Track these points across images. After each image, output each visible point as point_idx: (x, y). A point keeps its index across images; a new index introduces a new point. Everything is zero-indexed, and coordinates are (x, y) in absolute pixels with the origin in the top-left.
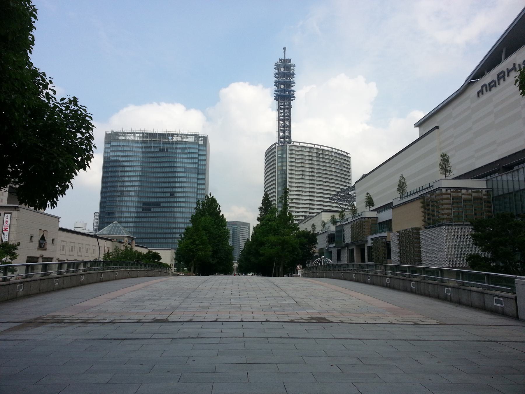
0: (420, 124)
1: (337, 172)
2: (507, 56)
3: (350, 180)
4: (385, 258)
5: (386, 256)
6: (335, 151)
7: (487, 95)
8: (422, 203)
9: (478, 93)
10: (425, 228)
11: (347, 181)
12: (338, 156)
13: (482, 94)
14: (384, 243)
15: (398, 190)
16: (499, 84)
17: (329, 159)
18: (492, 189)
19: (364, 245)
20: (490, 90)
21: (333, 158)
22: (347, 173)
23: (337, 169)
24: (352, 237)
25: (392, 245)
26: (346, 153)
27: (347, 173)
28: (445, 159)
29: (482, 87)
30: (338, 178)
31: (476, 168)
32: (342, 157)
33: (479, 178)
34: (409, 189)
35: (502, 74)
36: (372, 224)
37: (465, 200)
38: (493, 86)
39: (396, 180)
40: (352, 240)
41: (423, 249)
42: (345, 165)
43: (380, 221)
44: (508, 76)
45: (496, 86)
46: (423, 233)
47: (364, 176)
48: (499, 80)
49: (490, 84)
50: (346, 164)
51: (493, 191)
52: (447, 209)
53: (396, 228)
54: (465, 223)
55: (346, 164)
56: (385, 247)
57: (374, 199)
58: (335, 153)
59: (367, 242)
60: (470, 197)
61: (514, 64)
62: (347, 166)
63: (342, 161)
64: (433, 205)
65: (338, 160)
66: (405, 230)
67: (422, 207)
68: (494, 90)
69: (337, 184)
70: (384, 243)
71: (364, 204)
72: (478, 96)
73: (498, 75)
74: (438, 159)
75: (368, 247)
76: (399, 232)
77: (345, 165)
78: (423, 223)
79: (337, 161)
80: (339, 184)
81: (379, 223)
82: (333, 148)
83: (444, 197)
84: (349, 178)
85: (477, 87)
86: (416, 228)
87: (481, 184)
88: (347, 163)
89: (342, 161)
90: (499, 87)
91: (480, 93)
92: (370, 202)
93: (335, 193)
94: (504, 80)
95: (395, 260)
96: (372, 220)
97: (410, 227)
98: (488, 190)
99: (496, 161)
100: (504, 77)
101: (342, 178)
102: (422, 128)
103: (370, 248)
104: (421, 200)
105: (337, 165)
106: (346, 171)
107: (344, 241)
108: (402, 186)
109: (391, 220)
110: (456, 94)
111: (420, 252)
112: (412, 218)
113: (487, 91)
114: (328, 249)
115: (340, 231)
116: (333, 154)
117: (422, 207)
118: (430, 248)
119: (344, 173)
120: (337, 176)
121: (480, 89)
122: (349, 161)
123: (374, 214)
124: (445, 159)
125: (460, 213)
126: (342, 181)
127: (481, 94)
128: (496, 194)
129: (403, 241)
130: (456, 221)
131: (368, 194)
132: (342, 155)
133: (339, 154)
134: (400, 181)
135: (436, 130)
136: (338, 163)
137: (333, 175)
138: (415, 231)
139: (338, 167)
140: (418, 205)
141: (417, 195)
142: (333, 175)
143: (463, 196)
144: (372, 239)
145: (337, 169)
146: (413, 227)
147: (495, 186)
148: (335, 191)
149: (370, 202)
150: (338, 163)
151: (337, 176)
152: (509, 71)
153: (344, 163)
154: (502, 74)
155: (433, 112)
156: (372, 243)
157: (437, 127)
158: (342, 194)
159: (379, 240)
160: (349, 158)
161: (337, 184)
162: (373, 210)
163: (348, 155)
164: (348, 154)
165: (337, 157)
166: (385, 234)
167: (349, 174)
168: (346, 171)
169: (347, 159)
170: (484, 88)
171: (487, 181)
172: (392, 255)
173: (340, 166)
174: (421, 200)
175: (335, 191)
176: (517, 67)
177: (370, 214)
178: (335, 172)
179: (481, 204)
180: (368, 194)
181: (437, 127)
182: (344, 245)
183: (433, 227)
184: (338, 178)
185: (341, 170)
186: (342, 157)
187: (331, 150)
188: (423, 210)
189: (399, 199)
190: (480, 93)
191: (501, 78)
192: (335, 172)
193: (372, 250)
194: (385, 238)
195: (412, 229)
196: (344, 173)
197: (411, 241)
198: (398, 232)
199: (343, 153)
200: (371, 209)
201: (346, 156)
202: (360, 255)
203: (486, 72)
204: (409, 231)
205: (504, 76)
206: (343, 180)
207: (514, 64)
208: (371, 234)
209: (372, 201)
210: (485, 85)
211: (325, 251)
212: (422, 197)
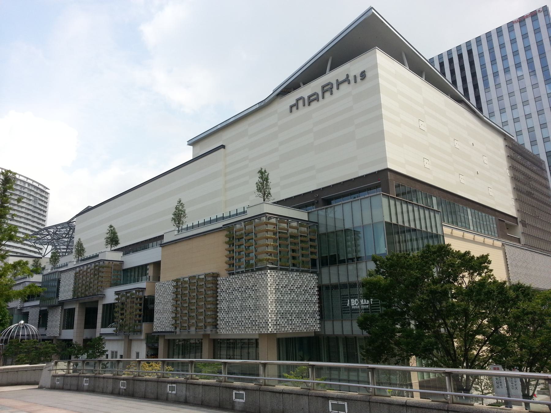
0: (194, 143)
1: (29, 209)
2: (332, 69)
3: (45, 221)
4: (139, 321)
5: (141, 318)
6: (31, 182)
7: (303, 111)
8: (226, 236)
9: (291, 107)
10: (230, 274)
11: (41, 217)
12: (33, 189)
13: (297, 109)
14: (141, 299)
15: (173, 219)
16: (323, 98)
17: (21, 191)
18: (317, 224)
19: (97, 302)
20: (309, 105)
21: (26, 190)
22: (42, 213)
23: (29, 205)
24: (74, 291)
25: (156, 301)
26: (45, 187)
27: (42, 213)
28: (264, 176)
29: (298, 100)
30: (29, 217)
31: (281, 199)
32: (39, 192)
33: (300, 207)
34: (188, 222)
35: (329, 86)
36: (114, 270)
37: (292, 236)
38: (313, 100)
39: (171, 205)
40: (74, 295)
41: (222, 305)
42: (41, 202)
43: (127, 266)
44: (338, 89)
45: (318, 101)
46: (223, 283)
47: (88, 209)
48: (323, 93)
49: (309, 97)
50: (42, 201)
51: (318, 227)
52: (267, 246)
53: (168, 275)
54: (301, 269)
55: (42, 201)
56: (141, 304)
57: (119, 235)
58: (29, 184)
59: (103, 297)
60: (295, 231)
61: (348, 76)
62: (43, 203)
63: (38, 196)
64: (243, 242)
65: (32, 193)
66: (190, 278)
67: (226, 243)
68: (314, 104)
69: (27, 224)
70: (141, 299)
71: (104, 241)
72: (291, 111)
73: (323, 87)
74: (257, 178)
75: (104, 305)
76: (177, 281)
77: (41, 202)
78: (227, 266)
79: (31, 195)
80: (29, 225)
81: (124, 270)
82: (27, 178)
83: (270, 227)
84: (44, 218)
85: (291, 98)
86: (213, 274)
87: (302, 215)
88: (43, 199)
89: (38, 196)
90: (322, 102)
91: (294, 107)
92: (113, 239)
93: (37, 230)
94: (332, 94)
95: (163, 320)
96: (115, 265)
97: (203, 272)
98: (312, 225)
99: (313, 191)
100: (331, 90)
101: (34, 217)
102: (198, 147)
103: (109, 308)
104: (226, 233)
105: (30, 200)
106: (41, 210)
107: (58, 296)
108: (178, 216)
109: (160, 261)
110: (257, 106)
111: (216, 311)
112: (210, 258)
113: (304, 105)
114: (21, 310)
115: (52, 284)
116: (26, 186)
117: (226, 243)
118: (237, 304)
119: (39, 211)
120: (28, 214)
121: (294, 102)
122: (47, 198)
123: (118, 256)
124: (264, 176)
125: (119, 281)
126: (34, 222)
127: (294, 109)
128: (322, 230)
129: (183, 295)
130: (287, 262)
131: (111, 226)
132: (38, 188)
133: (35, 187)
134: (176, 208)
135: (222, 150)
136: (31, 198)
137: (22, 212)
138: (210, 279)
139: (31, 203)
140: (221, 238)
141: (219, 225)
142: (22, 212)
143: (290, 230)
144: (117, 293)
145: (29, 205)
146: (207, 272)
147: (322, 221)
148: (37, 228)
149: (113, 239)
150: (31, 198)
151: (28, 214)
152: (339, 84)
153: (40, 199)
154: (329, 86)
155: (219, 127)
156: (116, 299)
157: (223, 147)
158: (38, 236)
159: (133, 294)
160: (48, 193)
161: (27, 224)
162: (115, 250)
163: (47, 190)
164: (47, 188)
165: (31, 190)
166: (142, 285)
167: (44, 214)
168: (41, 210)
169: (44, 194)
170: (301, 103)
171: (308, 213)
172: (156, 316)
173: (34, 202)
174: (226, 233)
175: (37, 228)
176: (351, 78)
177: (112, 255)
178: (26, 208)
179: (286, 239)
180: (111, 226)
181: (223, 147)
182: (57, 303)
183: (247, 271)
184: (29, 217)
185: (35, 207)
186: (39, 192)
187: (25, 180)
188: (227, 246)
189: (176, 233)
190: (294, 107)
191: (327, 91)
192: (26, 208)
193: (116, 310)
194: (143, 290)
195: (206, 275)
196: (39, 211)
197: (198, 295)
198: (174, 281)
199: (40, 187)
200: (113, 249)
201: (43, 191)
202: (83, 318)
203: (301, 84)
204: (186, 282)
205: (332, 88)
206: (35, 220)
207: (348, 76)
208: (116, 285)
209: (117, 237)
210: (302, 98)
211: (16, 312)
212: (228, 228)
